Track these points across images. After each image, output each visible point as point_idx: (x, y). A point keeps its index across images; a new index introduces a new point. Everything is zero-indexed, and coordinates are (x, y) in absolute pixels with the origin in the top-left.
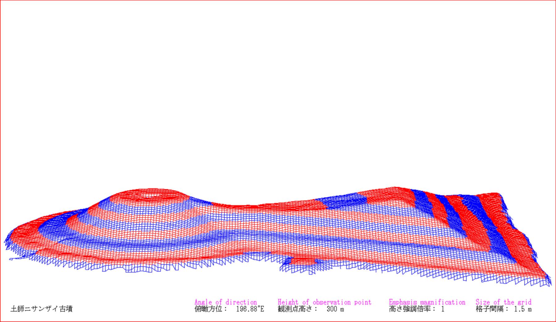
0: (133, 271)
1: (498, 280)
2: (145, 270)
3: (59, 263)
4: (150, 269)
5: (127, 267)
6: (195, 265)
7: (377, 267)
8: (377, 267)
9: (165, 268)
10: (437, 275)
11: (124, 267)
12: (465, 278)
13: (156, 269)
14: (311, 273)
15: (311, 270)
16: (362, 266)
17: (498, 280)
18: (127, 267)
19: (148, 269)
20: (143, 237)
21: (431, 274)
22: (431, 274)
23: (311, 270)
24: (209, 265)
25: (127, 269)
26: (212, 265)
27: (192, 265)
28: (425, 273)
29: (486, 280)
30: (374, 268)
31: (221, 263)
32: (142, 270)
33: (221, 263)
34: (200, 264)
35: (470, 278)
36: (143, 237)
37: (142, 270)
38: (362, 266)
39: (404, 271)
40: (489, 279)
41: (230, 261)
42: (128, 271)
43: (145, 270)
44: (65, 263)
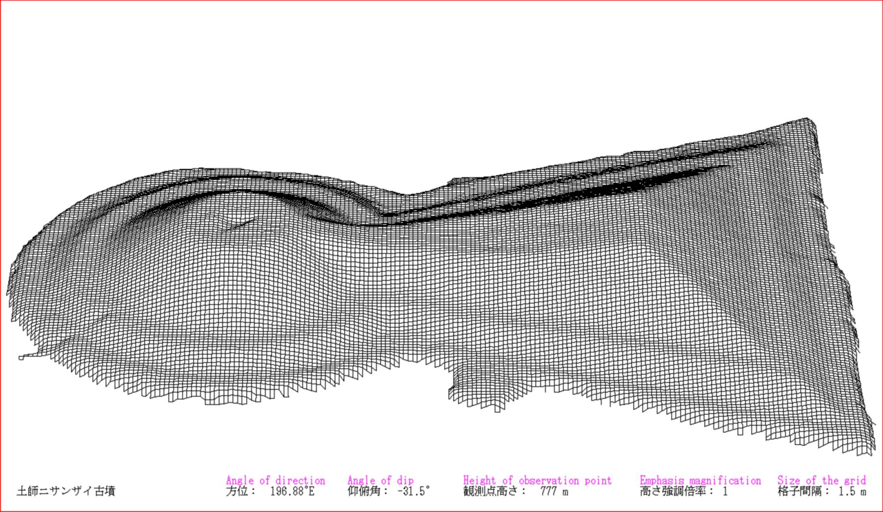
0: (217, 401)
1: (793, 437)
2: (235, 401)
3: (100, 379)
4: (244, 399)
5: (208, 394)
6: (314, 386)
7: (745, 424)
8: (745, 424)
9: (268, 395)
10: (698, 419)
11: (203, 394)
12: (740, 430)
13: (254, 397)
14: (498, 409)
15: (497, 403)
16: (580, 390)
17: (793, 437)
18: (208, 394)
19: (240, 398)
20: (168, 364)
21: (688, 417)
22: (688, 417)
23: (497, 403)
24: (337, 381)
25: (208, 398)
26: (341, 380)
27: (309, 386)
28: (571, 386)
29: (773, 436)
30: (543, 383)
31: (355, 376)
32: (231, 400)
33: (355, 376)
34: (323, 382)
35: (747, 430)
36: (168, 364)
37: (231, 400)
38: (580, 390)
39: (645, 406)
40: (778, 435)
41: (369, 369)
42: (210, 402)
43: (235, 401)
44: (108, 379)
